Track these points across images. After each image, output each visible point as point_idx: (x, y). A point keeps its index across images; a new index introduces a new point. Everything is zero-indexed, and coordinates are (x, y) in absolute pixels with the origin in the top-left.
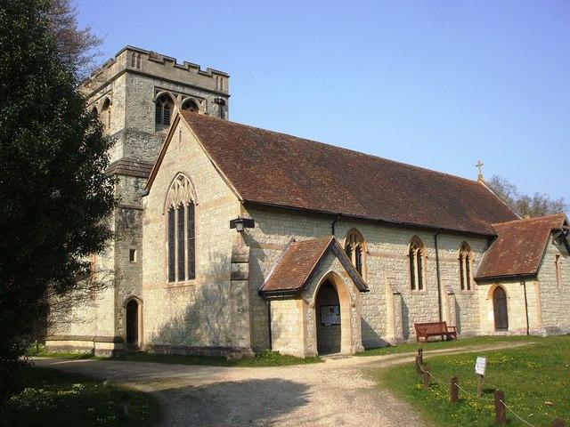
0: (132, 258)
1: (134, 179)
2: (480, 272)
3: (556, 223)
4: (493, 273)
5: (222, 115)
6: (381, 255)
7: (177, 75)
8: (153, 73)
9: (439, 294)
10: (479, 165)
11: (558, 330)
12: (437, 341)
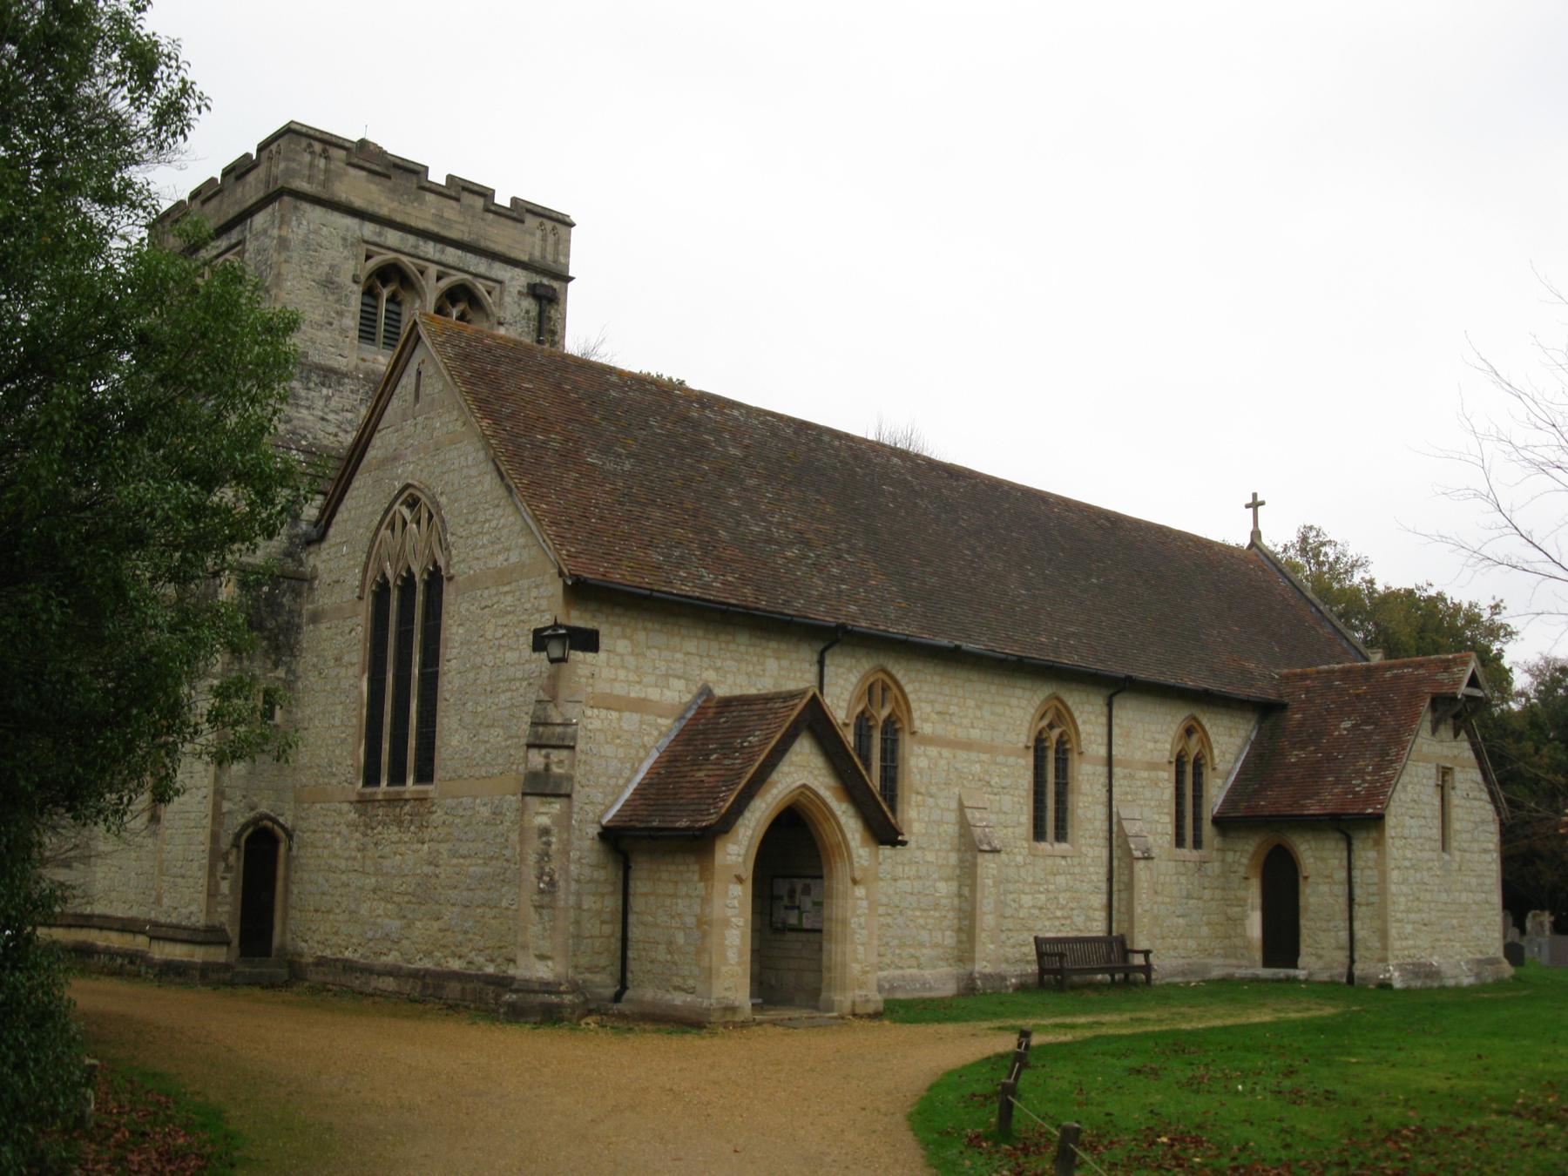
2: (1230, 801)
4: (1264, 805)
7: (424, 214)
8: (358, 202)
10: (1255, 504)
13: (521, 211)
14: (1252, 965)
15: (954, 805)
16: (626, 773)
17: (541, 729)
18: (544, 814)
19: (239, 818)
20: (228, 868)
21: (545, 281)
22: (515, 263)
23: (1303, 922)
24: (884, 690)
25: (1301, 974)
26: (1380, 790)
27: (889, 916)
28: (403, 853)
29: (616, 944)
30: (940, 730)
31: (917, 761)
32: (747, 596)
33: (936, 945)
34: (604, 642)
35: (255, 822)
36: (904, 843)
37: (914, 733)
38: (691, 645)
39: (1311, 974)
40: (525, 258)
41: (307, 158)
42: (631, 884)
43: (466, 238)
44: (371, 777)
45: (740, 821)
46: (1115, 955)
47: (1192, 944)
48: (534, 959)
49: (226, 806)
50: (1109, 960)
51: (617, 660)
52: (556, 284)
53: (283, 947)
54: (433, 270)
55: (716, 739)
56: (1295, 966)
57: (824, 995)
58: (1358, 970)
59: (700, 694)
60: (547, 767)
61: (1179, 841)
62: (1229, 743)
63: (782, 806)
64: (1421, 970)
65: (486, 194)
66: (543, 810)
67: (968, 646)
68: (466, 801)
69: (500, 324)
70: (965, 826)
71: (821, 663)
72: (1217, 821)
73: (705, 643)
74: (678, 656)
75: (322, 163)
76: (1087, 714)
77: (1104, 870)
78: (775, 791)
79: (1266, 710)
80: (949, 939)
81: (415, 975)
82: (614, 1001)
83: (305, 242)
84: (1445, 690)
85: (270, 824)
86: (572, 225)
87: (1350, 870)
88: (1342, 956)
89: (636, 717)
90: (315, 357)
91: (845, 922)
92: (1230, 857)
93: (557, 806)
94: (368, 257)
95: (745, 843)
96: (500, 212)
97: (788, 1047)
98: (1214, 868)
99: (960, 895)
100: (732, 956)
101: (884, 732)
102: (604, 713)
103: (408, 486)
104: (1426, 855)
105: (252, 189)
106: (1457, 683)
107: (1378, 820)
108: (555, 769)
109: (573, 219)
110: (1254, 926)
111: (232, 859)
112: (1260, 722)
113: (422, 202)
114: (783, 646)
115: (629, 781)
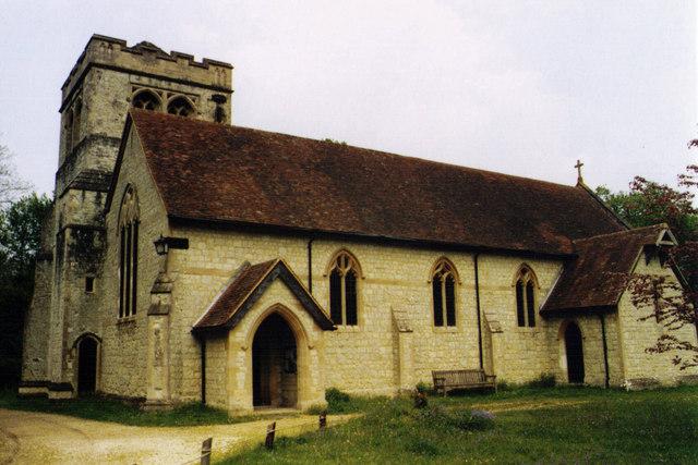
0: (89, 287)
5: (220, 115)
6: (385, 282)
7: (162, 68)
8: (128, 67)
9: (480, 336)
10: (579, 166)
13: (207, 64)
15: (388, 311)
20: (71, 357)
23: (585, 360)
26: (615, 297)
27: (332, 364)
30: (378, 276)
34: (191, 244)
37: (363, 278)
38: (238, 243)
40: (210, 84)
41: (102, 49)
49: (70, 330)
51: (199, 252)
52: (225, 95)
54: (165, 93)
61: (521, 323)
62: (546, 278)
65: (190, 58)
69: (199, 113)
70: (394, 321)
71: (476, 264)
75: (110, 51)
76: (463, 268)
77: (477, 339)
78: (262, 307)
79: (567, 261)
84: (649, 243)
86: (232, 68)
87: (604, 333)
88: (603, 376)
89: (210, 277)
90: (109, 135)
92: (550, 330)
93: (162, 319)
94: (134, 89)
98: (542, 335)
100: (241, 385)
102: (192, 276)
106: (656, 239)
111: (74, 352)
113: (158, 64)
114: (288, 241)
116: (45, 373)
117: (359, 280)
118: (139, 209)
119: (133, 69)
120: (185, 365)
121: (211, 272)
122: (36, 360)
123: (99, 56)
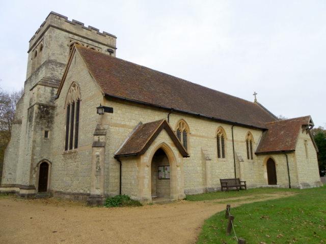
1: (51, 88)
2: (259, 148)
3: (304, 121)
4: (266, 150)
7: (84, 33)
8: (68, 30)
10: (255, 94)
11: (308, 185)
12: (234, 190)
13: (105, 34)
14: (266, 184)
15: (200, 150)
16: (121, 142)
17: (98, 131)
18: (98, 151)
19: (38, 160)
20: (35, 171)
21: (111, 49)
22: (104, 45)
24: (183, 124)
25: (278, 186)
26: (294, 144)
27: (186, 174)
28: (72, 164)
29: (119, 184)
31: (191, 140)
32: (150, 101)
33: (198, 182)
34: (114, 111)
35: (42, 161)
36: (189, 157)
39: (280, 186)
42: (122, 169)
43: (93, 39)
44: (66, 149)
45: (147, 151)
46: (237, 181)
47: (253, 180)
48: (95, 189)
49: (35, 157)
50: (236, 184)
53: (49, 190)
55: (144, 134)
56: (276, 184)
57: (171, 195)
58: (291, 184)
59: (139, 124)
60: (99, 140)
61: (248, 158)
62: (257, 136)
63: (158, 148)
64: (305, 184)
65: (97, 30)
66: (98, 151)
67: (201, 114)
68: (84, 151)
70: (203, 154)
72: (255, 154)
73: (140, 112)
74: (134, 115)
75: (59, 21)
76: (227, 129)
77: (233, 164)
80: (201, 180)
81: (74, 194)
82: (120, 201)
83: (56, 37)
85: (46, 161)
90: (58, 61)
91: (175, 176)
92: (259, 161)
93: (101, 149)
94: (71, 41)
95: (149, 157)
96: (100, 34)
97: (161, 211)
99: (203, 170)
100: (146, 186)
101: (184, 133)
102: (115, 128)
103: (74, 82)
104: (304, 159)
105: (45, 27)
106: (307, 122)
107: (293, 151)
108: (101, 141)
109: (117, 37)
110: (266, 176)
111: (36, 169)
112: (263, 133)
115: (122, 144)
116: (15, 180)
117: (188, 135)
118: (80, 94)
119: (71, 31)
120: (110, 175)
121: (123, 126)
122: (10, 174)
123: (54, 22)
